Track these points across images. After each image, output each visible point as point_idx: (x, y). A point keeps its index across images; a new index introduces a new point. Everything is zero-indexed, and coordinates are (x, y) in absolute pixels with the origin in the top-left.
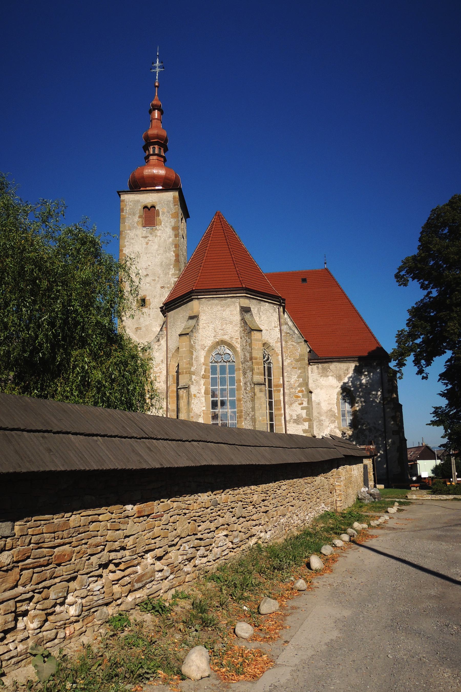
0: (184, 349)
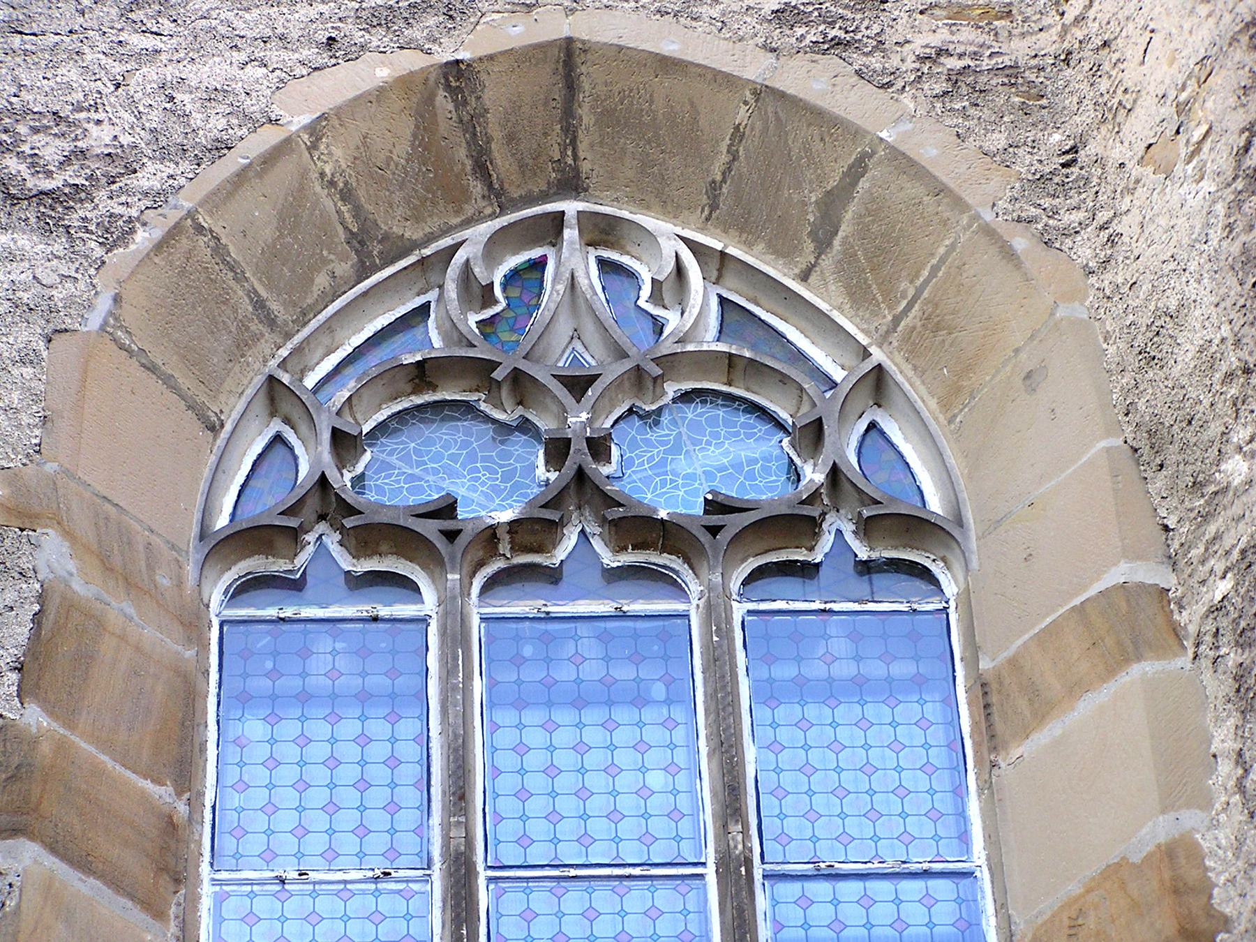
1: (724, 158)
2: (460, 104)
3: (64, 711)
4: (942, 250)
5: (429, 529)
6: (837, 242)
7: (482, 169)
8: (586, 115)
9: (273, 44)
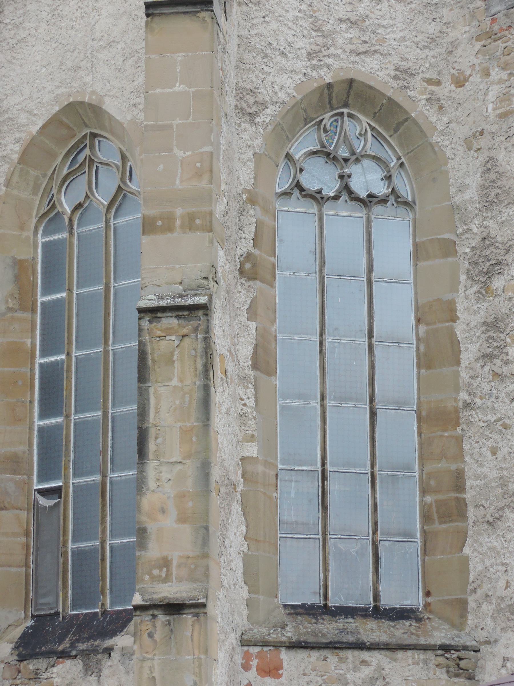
0: (179, 88)
1: (379, 108)
2: (329, 91)
3: (260, 250)
4: (420, 143)
5: (318, 196)
6: (398, 132)
7: (330, 103)
8: (352, 92)
9: (293, 73)
